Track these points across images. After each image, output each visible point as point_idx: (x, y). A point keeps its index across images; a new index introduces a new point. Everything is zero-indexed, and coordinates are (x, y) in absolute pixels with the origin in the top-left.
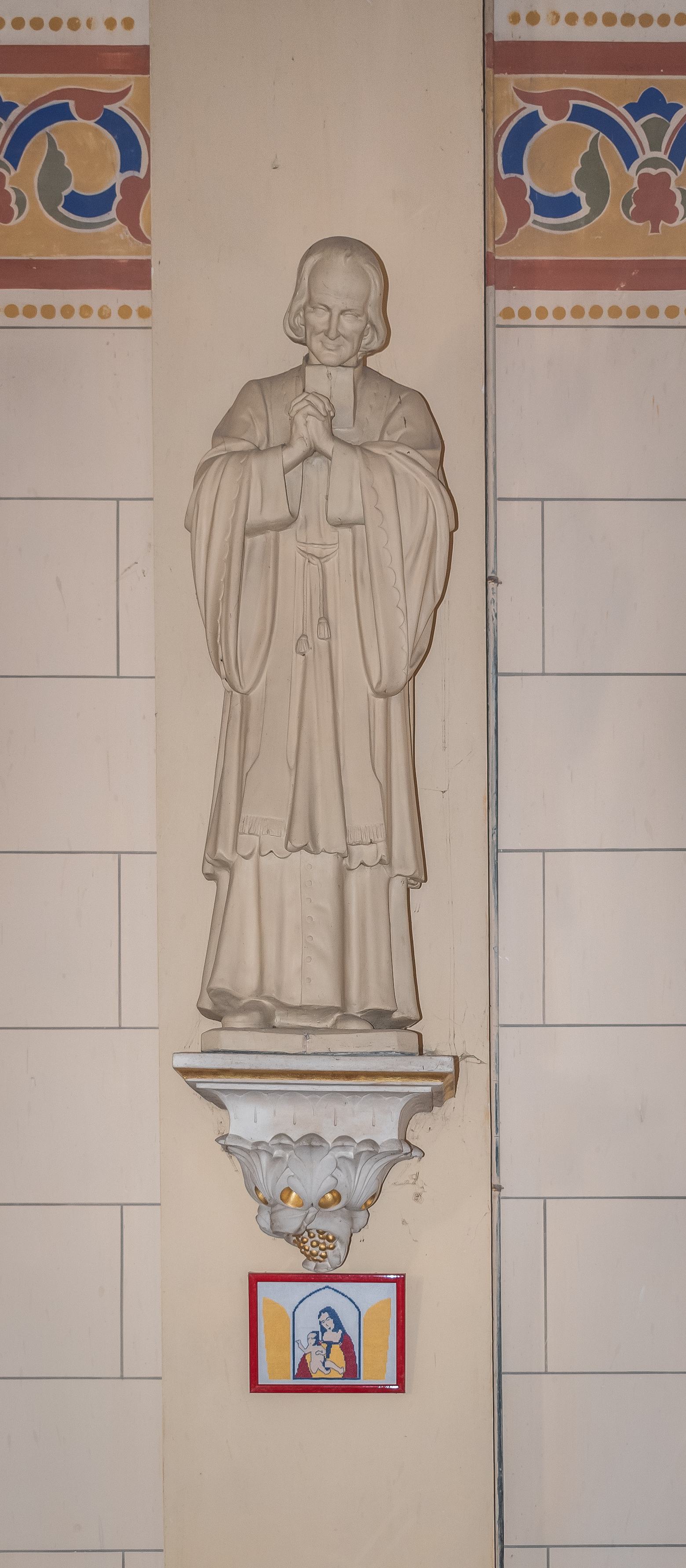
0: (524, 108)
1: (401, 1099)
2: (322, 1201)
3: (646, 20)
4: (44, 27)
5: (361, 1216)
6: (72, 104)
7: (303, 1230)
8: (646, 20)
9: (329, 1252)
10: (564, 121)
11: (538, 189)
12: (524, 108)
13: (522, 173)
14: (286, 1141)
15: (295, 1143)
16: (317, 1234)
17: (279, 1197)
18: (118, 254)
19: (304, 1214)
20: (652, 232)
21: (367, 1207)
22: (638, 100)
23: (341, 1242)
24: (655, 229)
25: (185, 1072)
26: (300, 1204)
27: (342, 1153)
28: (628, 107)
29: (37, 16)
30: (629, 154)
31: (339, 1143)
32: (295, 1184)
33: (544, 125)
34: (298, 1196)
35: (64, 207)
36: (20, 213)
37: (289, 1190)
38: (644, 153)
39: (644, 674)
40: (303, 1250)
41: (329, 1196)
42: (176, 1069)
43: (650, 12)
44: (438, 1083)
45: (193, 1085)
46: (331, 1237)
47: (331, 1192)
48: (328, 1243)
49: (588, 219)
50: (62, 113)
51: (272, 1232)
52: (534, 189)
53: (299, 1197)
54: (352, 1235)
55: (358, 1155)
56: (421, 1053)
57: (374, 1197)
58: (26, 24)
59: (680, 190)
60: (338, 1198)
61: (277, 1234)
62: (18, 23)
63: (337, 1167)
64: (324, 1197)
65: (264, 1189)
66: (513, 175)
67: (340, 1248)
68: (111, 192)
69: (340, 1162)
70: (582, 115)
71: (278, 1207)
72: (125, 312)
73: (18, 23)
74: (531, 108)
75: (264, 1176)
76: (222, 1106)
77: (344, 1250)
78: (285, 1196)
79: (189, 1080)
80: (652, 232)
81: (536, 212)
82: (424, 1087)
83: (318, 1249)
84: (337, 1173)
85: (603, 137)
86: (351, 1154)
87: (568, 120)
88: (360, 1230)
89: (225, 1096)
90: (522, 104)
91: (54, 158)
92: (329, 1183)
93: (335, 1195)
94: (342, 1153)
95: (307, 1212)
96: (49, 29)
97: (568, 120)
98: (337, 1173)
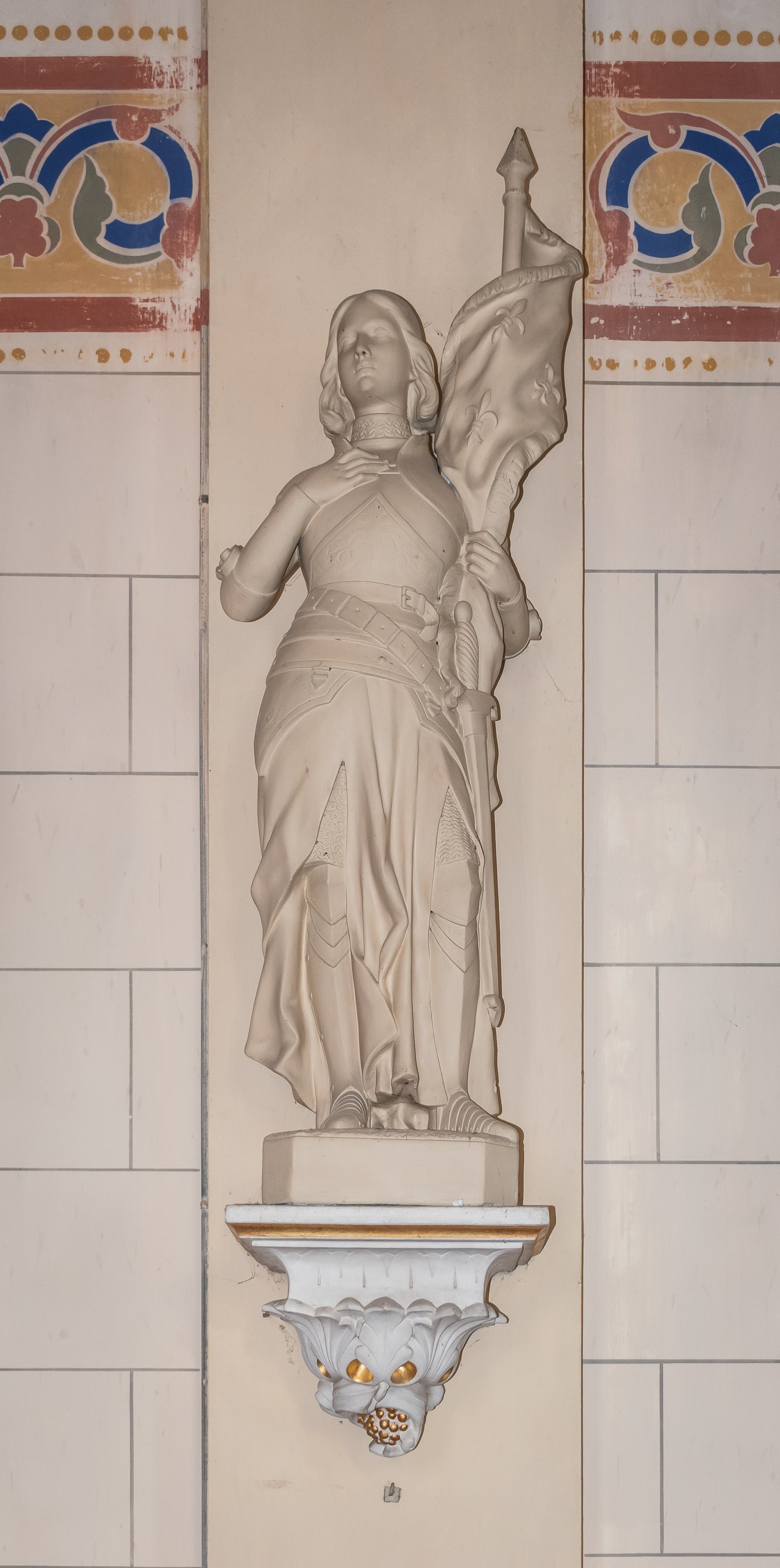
0: (629, 134)
1: (487, 1257)
2: (395, 1375)
3: (42, 33)
4: (93, 36)
5: (437, 1391)
6: (114, 122)
7: (372, 1408)
8: (63, 33)
9: (400, 1433)
10: (137, 143)
11: (642, 224)
12: (629, 134)
13: (627, 207)
14: (352, 1306)
15: (365, 1308)
16: (387, 1413)
17: (346, 1374)
18: (765, 301)
19: (372, 1390)
20: (15, 265)
21: (442, 1381)
22: (760, 127)
23: (414, 1421)
24: (19, 262)
25: (239, 1228)
26: (368, 1379)
27: (419, 1319)
28: (750, 136)
29: (58, 25)
30: (749, 187)
31: (417, 1308)
32: (363, 1354)
33: (654, 152)
34: (367, 1368)
35: (106, 238)
36: (53, 245)
37: (356, 1363)
38: (764, 186)
39: (618, 765)
40: (371, 1432)
41: (402, 1369)
42: (229, 1224)
43: (749, 29)
44: (532, 1238)
45: (245, 1244)
46: (403, 1416)
47: (404, 1365)
48: (400, 1424)
49: (697, 259)
50: (103, 132)
51: (334, 1410)
52: (640, 224)
53: (367, 1371)
54: (426, 1413)
55: (438, 1322)
56: (520, 1203)
57: (452, 1371)
58: (756, 37)
59: (47, 221)
60: (412, 1371)
61: (339, 1413)
62: (20, 33)
63: (413, 1336)
64: (397, 1371)
65: (328, 1361)
66: (617, 208)
67: (413, 1431)
68: (158, 223)
69: (417, 1329)
70: (695, 142)
71: (342, 1382)
72: (670, 364)
73: (20, 33)
74: (638, 134)
75: (329, 1350)
76: (276, 1268)
77: (418, 1432)
78: (351, 1371)
79: (241, 1237)
80: (15, 265)
81: (640, 250)
82: (515, 1243)
83: (380, 1429)
84: (414, 1343)
85: (716, 165)
86: (428, 1320)
87: (681, 148)
88: (435, 1407)
89: (285, 1256)
90: (629, 129)
91: (94, 184)
92: (403, 1354)
93: (410, 1367)
94: (419, 1319)
95: (377, 1387)
96: (97, 38)
97: (681, 148)
98: (414, 1343)
